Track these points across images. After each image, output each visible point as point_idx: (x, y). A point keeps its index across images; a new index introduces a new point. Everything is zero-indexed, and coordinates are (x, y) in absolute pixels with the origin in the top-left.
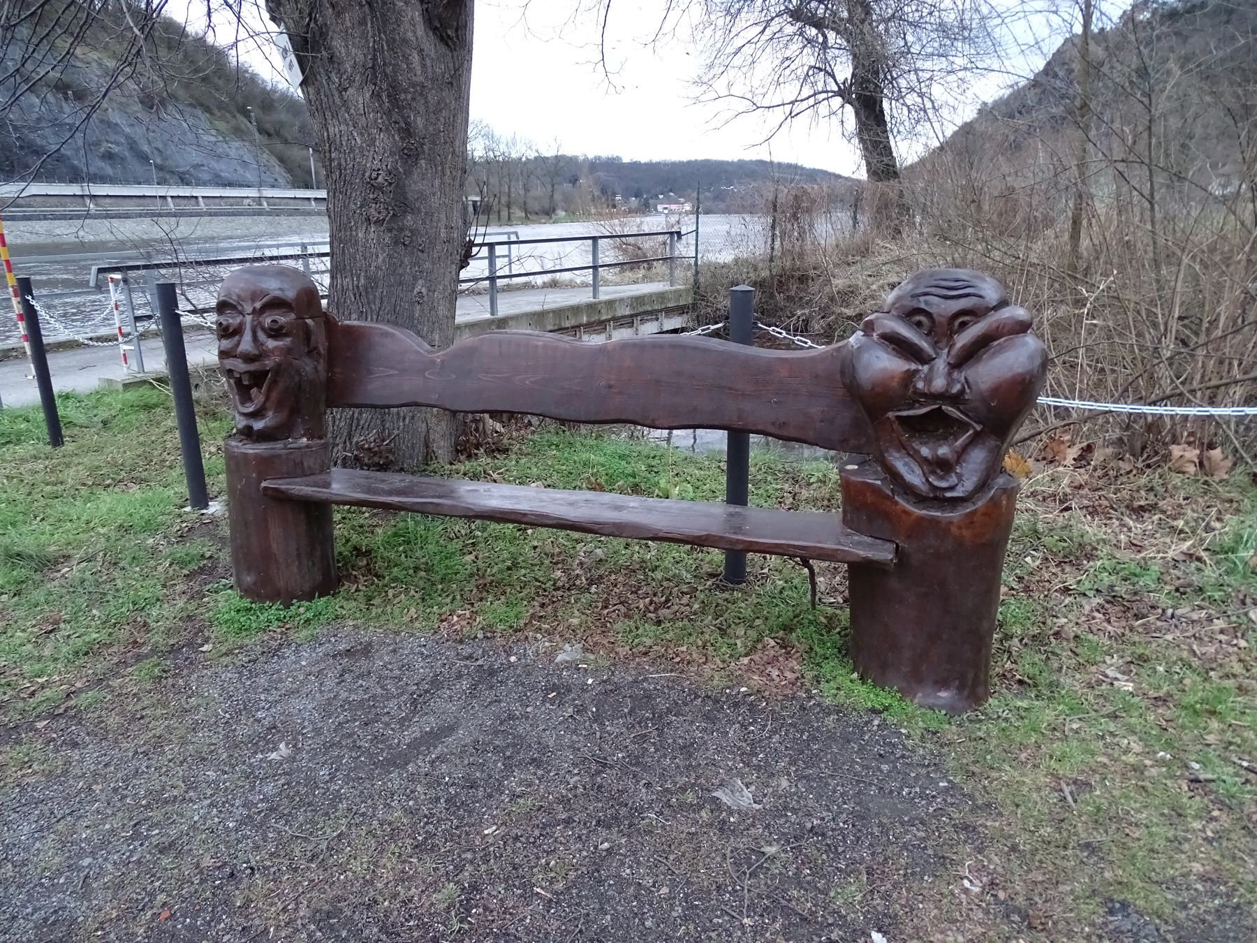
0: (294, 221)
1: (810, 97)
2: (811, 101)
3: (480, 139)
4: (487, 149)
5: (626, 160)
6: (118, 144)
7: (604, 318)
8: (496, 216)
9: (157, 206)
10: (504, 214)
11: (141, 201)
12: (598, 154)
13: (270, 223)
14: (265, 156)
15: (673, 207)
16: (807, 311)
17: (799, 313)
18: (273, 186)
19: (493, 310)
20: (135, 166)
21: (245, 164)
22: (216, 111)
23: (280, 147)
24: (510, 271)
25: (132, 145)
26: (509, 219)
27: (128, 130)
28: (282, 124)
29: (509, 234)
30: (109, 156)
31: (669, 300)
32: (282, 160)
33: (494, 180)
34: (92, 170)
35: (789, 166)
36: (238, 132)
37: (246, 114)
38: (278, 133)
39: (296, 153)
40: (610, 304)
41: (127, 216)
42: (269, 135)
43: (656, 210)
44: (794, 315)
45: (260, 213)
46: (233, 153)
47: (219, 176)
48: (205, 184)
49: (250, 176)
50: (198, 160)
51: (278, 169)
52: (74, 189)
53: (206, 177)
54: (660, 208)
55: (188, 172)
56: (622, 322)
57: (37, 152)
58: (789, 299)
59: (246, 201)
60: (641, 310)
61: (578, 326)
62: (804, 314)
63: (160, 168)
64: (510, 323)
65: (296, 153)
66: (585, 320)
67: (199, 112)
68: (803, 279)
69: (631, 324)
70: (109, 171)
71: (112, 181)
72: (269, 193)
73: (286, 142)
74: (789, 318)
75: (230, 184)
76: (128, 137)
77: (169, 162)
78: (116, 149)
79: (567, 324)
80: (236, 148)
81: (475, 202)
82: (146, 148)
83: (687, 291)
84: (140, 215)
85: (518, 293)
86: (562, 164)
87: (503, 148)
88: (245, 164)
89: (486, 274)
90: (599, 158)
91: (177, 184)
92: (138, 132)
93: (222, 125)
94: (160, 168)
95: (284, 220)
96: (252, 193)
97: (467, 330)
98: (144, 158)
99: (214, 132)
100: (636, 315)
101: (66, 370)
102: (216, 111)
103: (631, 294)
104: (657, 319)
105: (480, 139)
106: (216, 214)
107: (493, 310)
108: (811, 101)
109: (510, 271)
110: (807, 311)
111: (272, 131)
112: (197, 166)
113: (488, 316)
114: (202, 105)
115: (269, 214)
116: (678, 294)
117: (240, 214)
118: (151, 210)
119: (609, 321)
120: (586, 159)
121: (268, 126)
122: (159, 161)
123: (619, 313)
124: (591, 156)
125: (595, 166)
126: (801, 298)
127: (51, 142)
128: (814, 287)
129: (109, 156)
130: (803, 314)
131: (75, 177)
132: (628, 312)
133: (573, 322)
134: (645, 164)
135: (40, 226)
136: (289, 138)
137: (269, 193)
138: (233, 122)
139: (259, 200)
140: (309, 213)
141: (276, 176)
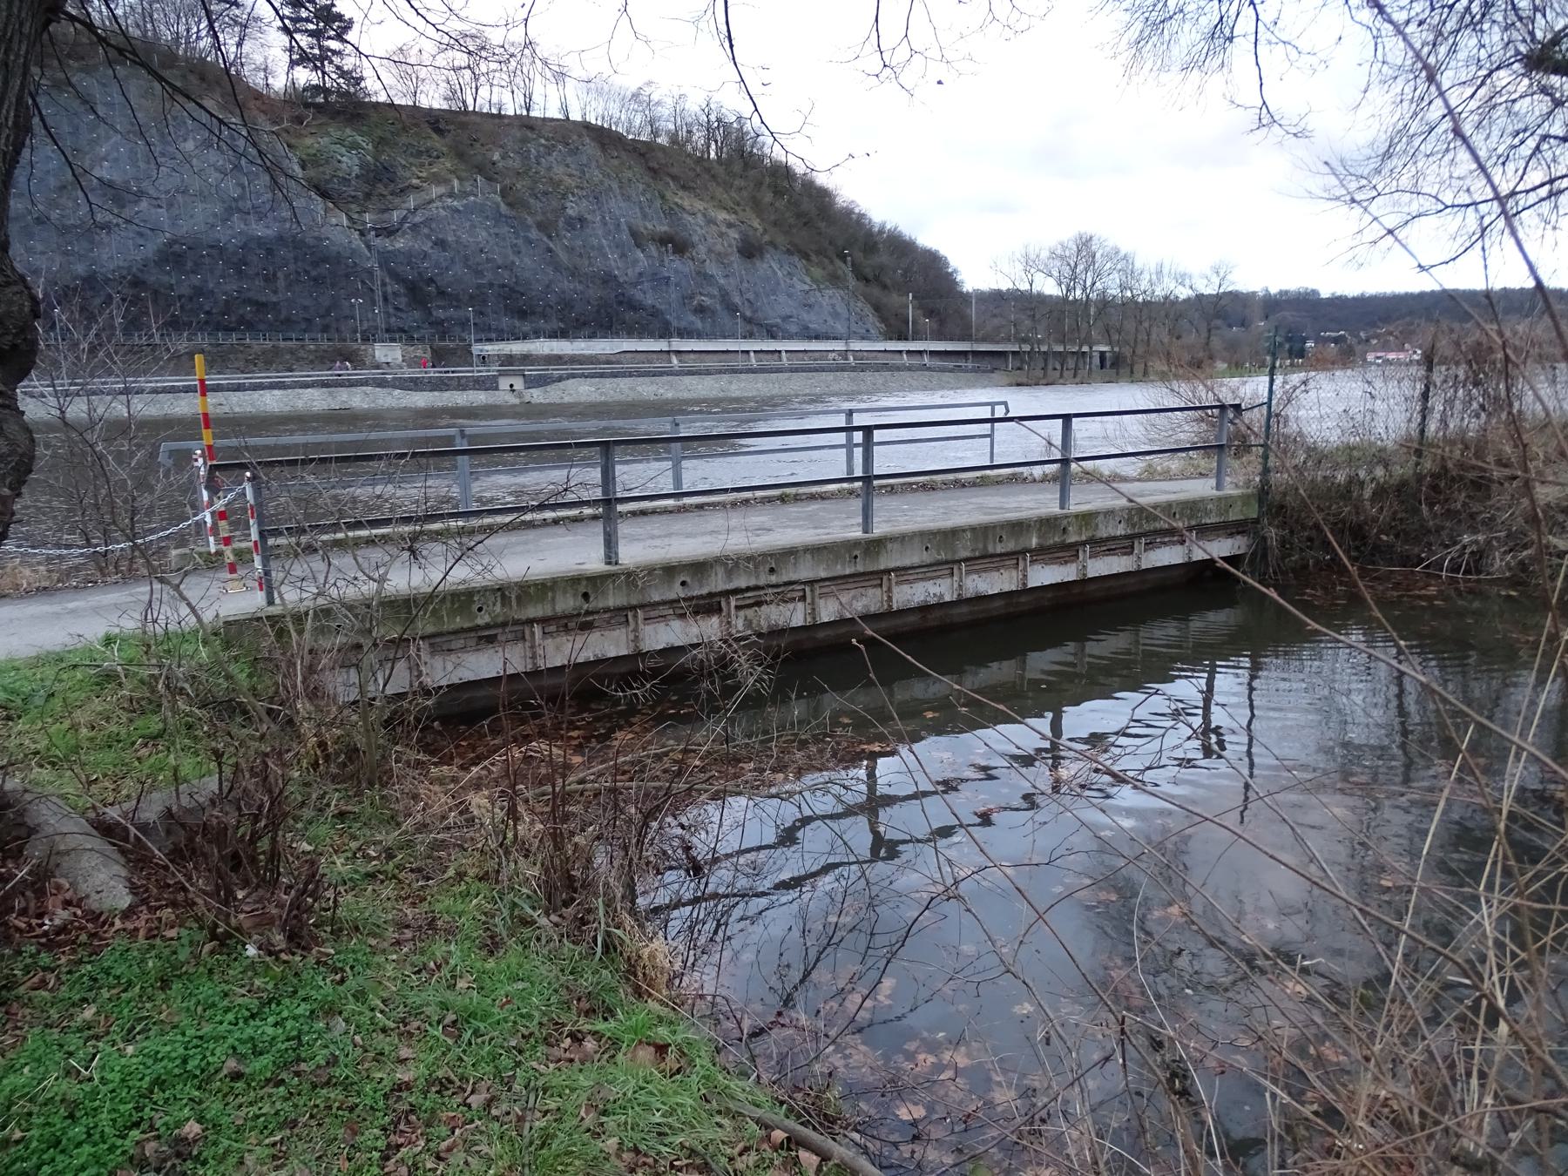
0: (879, 378)
1: (1542, 185)
2: (1544, 192)
3: (1115, 275)
4: (1123, 288)
5: (1325, 293)
6: (709, 295)
7: (1072, 539)
8: (1128, 370)
9: (739, 362)
10: (1139, 368)
11: (724, 356)
12: (1285, 288)
13: (853, 380)
14: (860, 305)
15: (1391, 356)
16: (1481, 538)
17: (1466, 538)
18: (863, 338)
19: (867, 525)
20: (724, 319)
21: (836, 315)
22: (814, 257)
23: (876, 291)
24: (678, 480)
25: (724, 296)
26: (1145, 373)
27: (722, 281)
28: (882, 268)
29: (993, 405)
30: (701, 310)
31: (1207, 513)
32: (877, 308)
33: (1130, 326)
34: (683, 324)
35: (900, 246)
36: (835, 280)
37: (843, 258)
38: (877, 278)
39: (894, 299)
40: (1087, 518)
41: (708, 373)
42: (867, 280)
43: (1365, 360)
44: (1455, 543)
45: (842, 369)
46: (825, 302)
47: (807, 328)
48: (789, 337)
49: (840, 328)
50: (788, 311)
51: (872, 319)
52: (662, 345)
53: (793, 329)
54: (1370, 357)
55: (776, 326)
56: (1103, 546)
57: (634, 306)
58: (1450, 514)
59: (831, 356)
60: (1146, 527)
61: (1023, 552)
62: (1476, 542)
63: (748, 321)
64: (889, 546)
65: (894, 299)
66: (1034, 542)
67: (796, 259)
68: (1481, 486)
69: (1129, 550)
70: (699, 325)
71: (699, 335)
72: (857, 345)
73: (885, 287)
74: (1447, 547)
75: (817, 337)
76: (721, 289)
77: (760, 314)
78: (707, 301)
79: (999, 549)
80: (830, 298)
81: (1102, 354)
82: (737, 300)
83: (1245, 499)
84: (720, 372)
85: (1003, 489)
86: (1223, 302)
87: (1144, 285)
88: (836, 315)
89: (598, 494)
90: (1286, 292)
91: (762, 338)
92: (730, 284)
93: (817, 272)
94: (748, 321)
95: (868, 377)
96: (839, 346)
97: (809, 556)
98: (732, 309)
99: (808, 280)
100: (1139, 536)
101: (633, 539)
102: (814, 257)
103: (1182, 497)
104: (1182, 542)
105: (1115, 275)
106: (796, 370)
107: (867, 525)
108: (1544, 192)
109: (678, 480)
110: (1481, 538)
111: (870, 276)
112: (786, 318)
113: (857, 533)
114: (799, 251)
115: (854, 369)
116: (1226, 503)
117: (823, 370)
118: (731, 365)
119: (1084, 544)
120: (1268, 295)
121: (868, 272)
122: (748, 314)
123: (1103, 532)
124: (1274, 290)
125: (1274, 305)
126: (1472, 516)
127: (648, 297)
128: (1500, 498)
129: (701, 310)
130: (1472, 542)
131: (665, 333)
132: (1121, 530)
133: (1010, 546)
134: (1354, 299)
135: (624, 384)
136: (888, 282)
137: (857, 345)
138: (831, 267)
139: (844, 354)
140: (898, 369)
141: (869, 326)
